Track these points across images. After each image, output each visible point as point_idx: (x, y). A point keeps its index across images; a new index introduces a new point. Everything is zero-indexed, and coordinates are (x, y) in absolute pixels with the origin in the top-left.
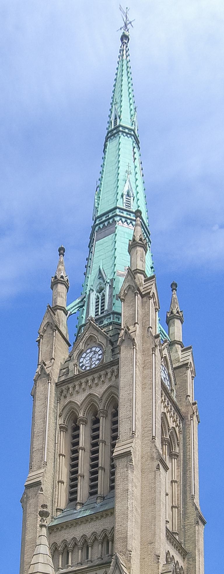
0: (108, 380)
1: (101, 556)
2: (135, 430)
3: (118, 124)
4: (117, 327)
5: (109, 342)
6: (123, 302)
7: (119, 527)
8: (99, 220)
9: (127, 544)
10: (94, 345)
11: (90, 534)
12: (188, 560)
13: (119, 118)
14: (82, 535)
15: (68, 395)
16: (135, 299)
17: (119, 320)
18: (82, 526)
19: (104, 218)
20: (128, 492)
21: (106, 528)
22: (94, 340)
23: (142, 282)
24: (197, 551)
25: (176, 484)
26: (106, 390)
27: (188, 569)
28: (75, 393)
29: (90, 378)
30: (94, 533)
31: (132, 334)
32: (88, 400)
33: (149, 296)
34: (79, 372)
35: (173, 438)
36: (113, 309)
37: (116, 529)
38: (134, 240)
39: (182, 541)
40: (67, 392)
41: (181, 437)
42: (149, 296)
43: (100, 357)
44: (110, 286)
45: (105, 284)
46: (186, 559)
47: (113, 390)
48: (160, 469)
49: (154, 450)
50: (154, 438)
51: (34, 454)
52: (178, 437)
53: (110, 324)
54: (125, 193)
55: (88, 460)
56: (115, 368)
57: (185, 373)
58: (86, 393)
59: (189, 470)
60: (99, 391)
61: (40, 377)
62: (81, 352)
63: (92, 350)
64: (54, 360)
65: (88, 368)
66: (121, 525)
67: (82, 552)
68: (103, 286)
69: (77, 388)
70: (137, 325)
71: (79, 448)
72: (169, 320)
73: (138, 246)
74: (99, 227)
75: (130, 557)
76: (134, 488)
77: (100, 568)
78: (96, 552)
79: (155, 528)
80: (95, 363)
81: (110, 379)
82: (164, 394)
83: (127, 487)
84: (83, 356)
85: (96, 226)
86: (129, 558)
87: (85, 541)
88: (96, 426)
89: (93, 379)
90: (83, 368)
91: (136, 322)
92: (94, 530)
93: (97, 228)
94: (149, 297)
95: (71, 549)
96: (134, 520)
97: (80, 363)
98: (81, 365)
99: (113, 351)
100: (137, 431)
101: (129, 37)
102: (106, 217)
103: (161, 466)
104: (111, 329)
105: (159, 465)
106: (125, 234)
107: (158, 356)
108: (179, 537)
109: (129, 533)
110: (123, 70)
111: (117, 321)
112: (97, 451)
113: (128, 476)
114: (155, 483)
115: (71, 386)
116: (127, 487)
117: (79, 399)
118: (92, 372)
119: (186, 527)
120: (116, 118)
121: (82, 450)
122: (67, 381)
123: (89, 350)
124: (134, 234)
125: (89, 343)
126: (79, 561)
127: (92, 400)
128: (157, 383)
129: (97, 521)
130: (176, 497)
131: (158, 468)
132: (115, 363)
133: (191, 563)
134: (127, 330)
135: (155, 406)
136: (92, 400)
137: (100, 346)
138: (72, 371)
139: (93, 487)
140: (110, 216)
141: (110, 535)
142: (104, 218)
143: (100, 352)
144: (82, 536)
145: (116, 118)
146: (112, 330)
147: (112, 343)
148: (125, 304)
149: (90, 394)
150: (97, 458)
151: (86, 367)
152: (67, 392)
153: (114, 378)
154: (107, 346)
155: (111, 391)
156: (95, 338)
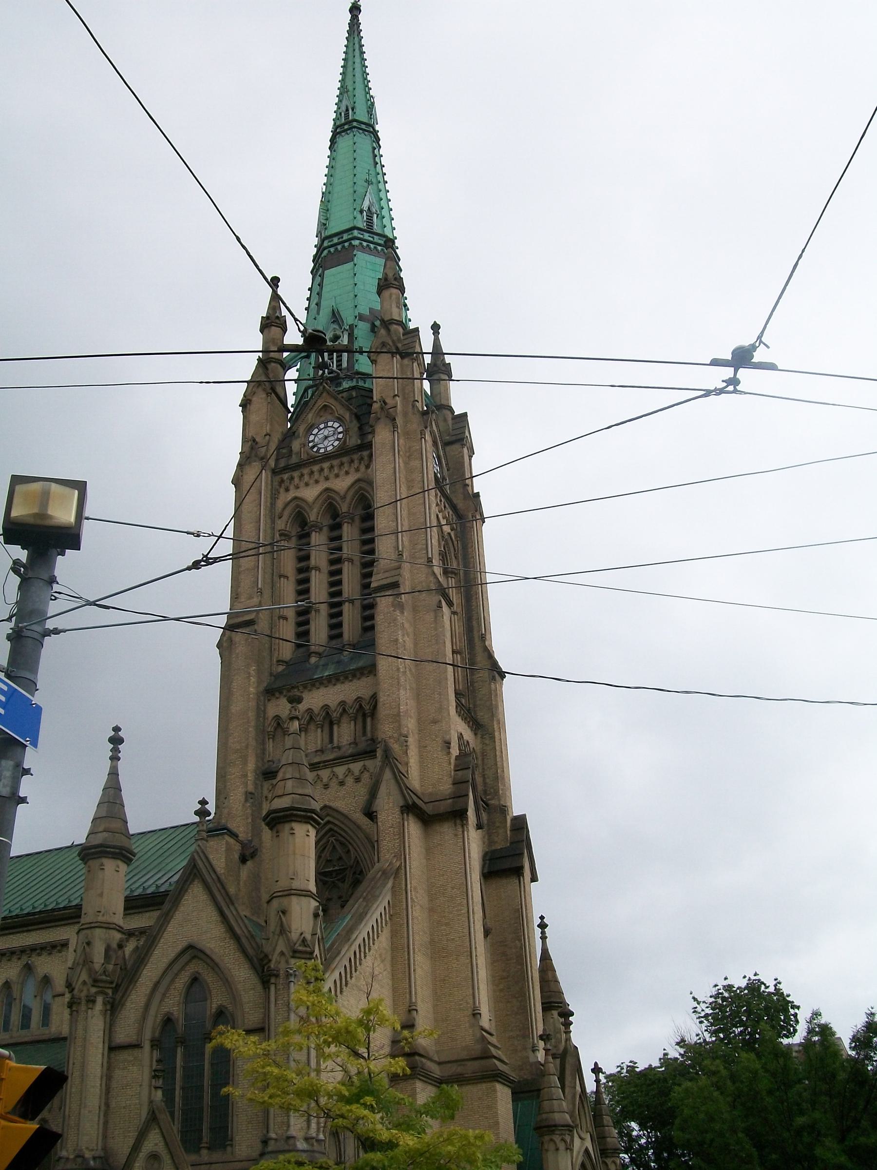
0: (354, 470)
1: (355, 739)
2: (403, 548)
3: (350, 118)
4: (363, 394)
5: (353, 416)
6: (374, 365)
7: (385, 698)
8: (329, 242)
9: (400, 725)
10: (330, 417)
11: (336, 703)
12: (482, 737)
13: (353, 110)
14: (321, 704)
15: (292, 487)
16: (393, 362)
17: (365, 384)
18: (321, 690)
19: (335, 240)
20: (397, 644)
21: (362, 696)
22: (330, 412)
23: (400, 337)
24: (495, 723)
25: (456, 616)
26: (353, 485)
27: (484, 754)
28: (302, 484)
29: (326, 465)
30: (343, 703)
31: (391, 410)
32: (325, 496)
33: (412, 357)
34: (308, 454)
35: (449, 547)
36: (356, 367)
37: (381, 700)
38: (386, 279)
39: (471, 706)
40: (290, 483)
41: (459, 545)
42: (412, 357)
43: (340, 436)
44: (349, 334)
45: (343, 332)
46: (479, 736)
47: (363, 485)
48: (442, 608)
49: (432, 579)
50: (430, 560)
51: (242, 576)
52: (456, 546)
53: (353, 388)
54: (364, 209)
55: (325, 585)
56: (365, 453)
57: (461, 452)
58: (322, 485)
59: (475, 596)
60: (342, 484)
61: (248, 461)
62: (311, 427)
63: (327, 424)
64: (270, 435)
65: (322, 451)
66: (388, 695)
67: (322, 731)
68: (339, 333)
69: (306, 478)
70: (397, 398)
71: (345, 601)
72: (382, 290)
73: (392, 287)
74: (329, 251)
75: (407, 746)
76: (406, 638)
77: (355, 761)
78: (345, 733)
79: (440, 698)
80: (332, 445)
81: (357, 470)
82: (439, 494)
83: (396, 636)
84: (313, 433)
85: (325, 250)
86: (405, 748)
87: (328, 713)
88: (335, 534)
89: (332, 467)
90: (315, 449)
91: (396, 393)
92: (341, 698)
93: (326, 252)
94: (412, 359)
95: (304, 728)
96: (408, 688)
97: (310, 442)
98: (311, 444)
99: (360, 428)
100: (405, 550)
101: (361, 8)
102: (339, 239)
103: (444, 603)
104: (354, 396)
105: (440, 601)
106: (368, 264)
107: (429, 441)
108: (466, 700)
109: (403, 708)
110: (354, 50)
111: (363, 384)
112: (339, 572)
113: (395, 619)
114: (436, 629)
115: (296, 474)
116: (396, 636)
117: (310, 493)
118: (328, 457)
119: (476, 684)
120: (347, 110)
121: (316, 570)
122: (290, 468)
123: (323, 425)
124: (387, 271)
125: (321, 415)
126: (319, 748)
127: (329, 497)
128: (430, 479)
129: (347, 683)
130: (457, 637)
131: (440, 606)
132: (367, 446)
133: (487, 742)
134: (383, 405)
135: (430, 513)
136: (329, 497)
137: (340, 419)
138: (297, 453)
139: (335, 627)
140: (344, 239)
141: (368, 707)
142: (335, 240)
143: (340, 429)
144: (322, 707)
145: (347, 110)
146: (357, 397)
147: (358, 417)
148: (377, 367)
149: (327, 490)
150: (339, 583)
151: (319, 449)
152: (290, 483)
153: (362, 468)
154: (351, 421)
155: (360, 487)
156: (332, 409)
